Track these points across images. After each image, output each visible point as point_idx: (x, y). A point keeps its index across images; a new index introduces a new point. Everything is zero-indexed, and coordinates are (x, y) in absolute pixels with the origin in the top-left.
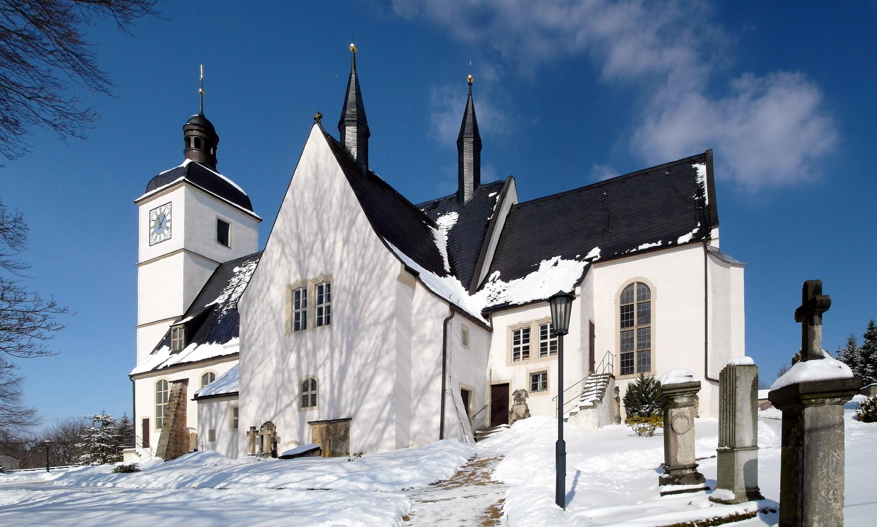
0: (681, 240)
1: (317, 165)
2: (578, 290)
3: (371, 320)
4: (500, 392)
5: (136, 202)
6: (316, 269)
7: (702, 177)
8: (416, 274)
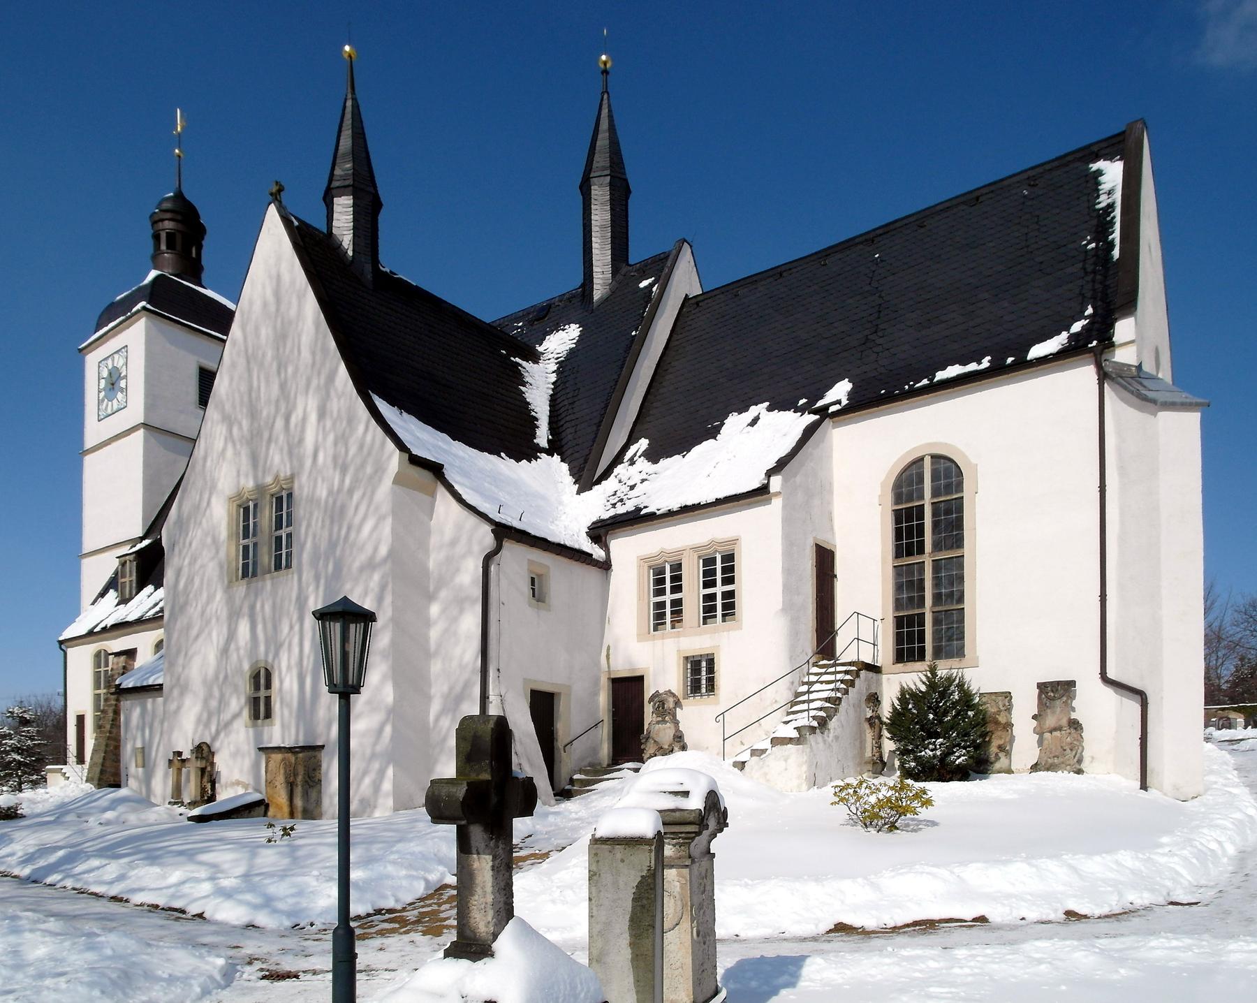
0: (1037, 351)
1: (279, 277)
2: (776, 483)
3: (362, 558)
4: (628, 690)
5: (80, 350)
6: (278, 463)
7: (1110, 193)
8: (436, 470)
